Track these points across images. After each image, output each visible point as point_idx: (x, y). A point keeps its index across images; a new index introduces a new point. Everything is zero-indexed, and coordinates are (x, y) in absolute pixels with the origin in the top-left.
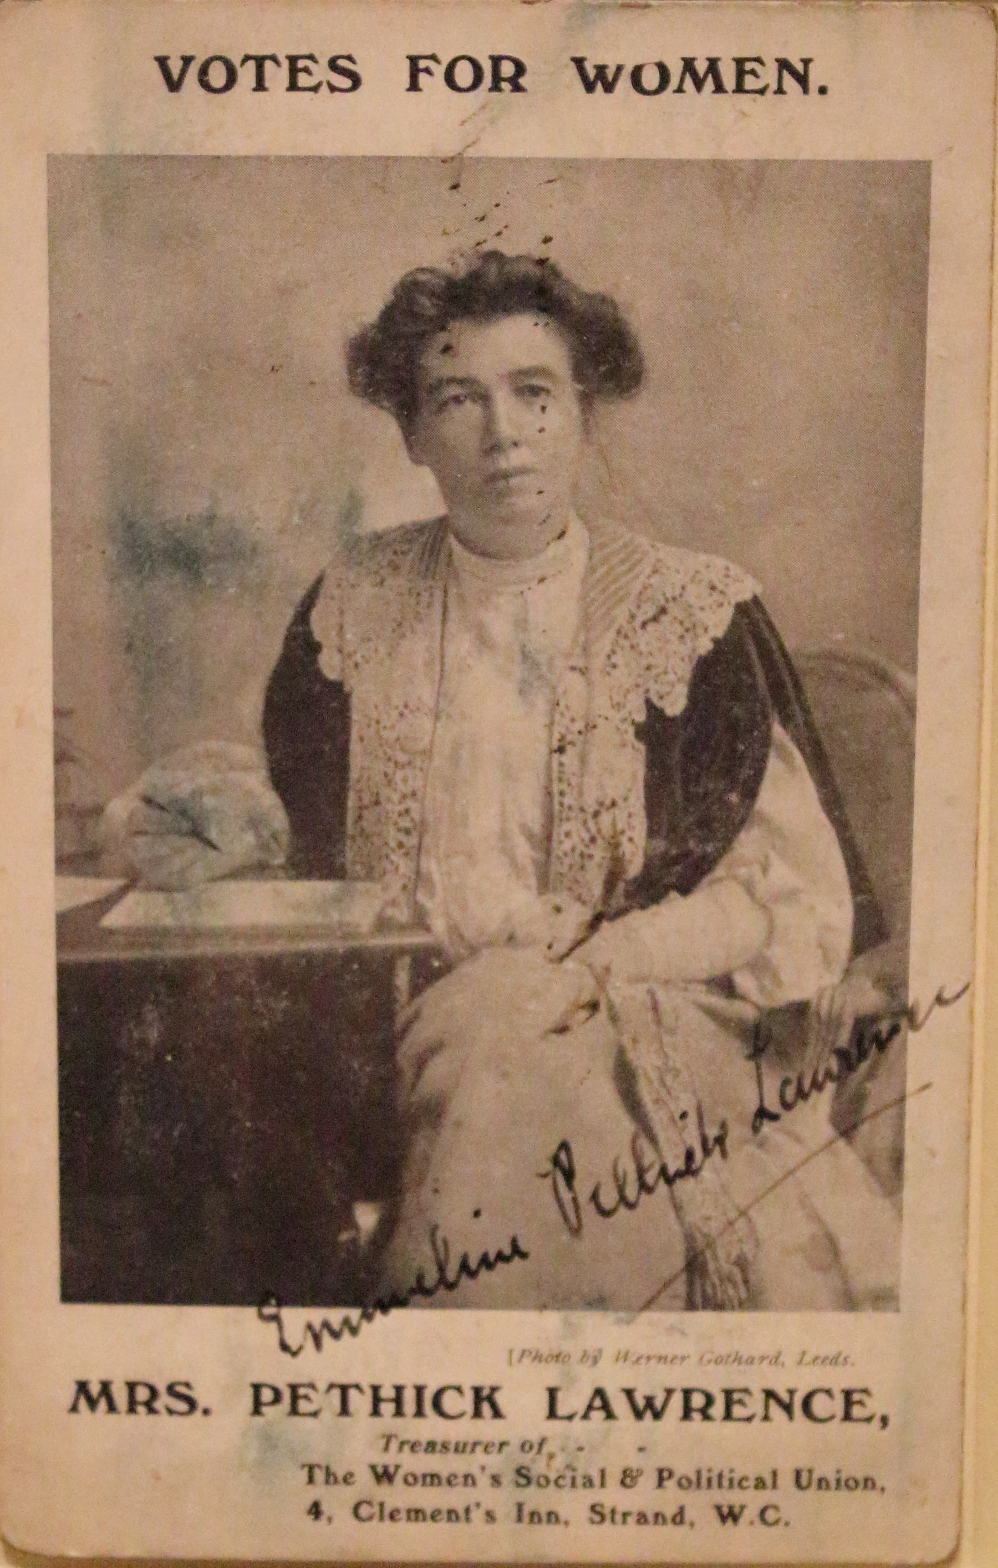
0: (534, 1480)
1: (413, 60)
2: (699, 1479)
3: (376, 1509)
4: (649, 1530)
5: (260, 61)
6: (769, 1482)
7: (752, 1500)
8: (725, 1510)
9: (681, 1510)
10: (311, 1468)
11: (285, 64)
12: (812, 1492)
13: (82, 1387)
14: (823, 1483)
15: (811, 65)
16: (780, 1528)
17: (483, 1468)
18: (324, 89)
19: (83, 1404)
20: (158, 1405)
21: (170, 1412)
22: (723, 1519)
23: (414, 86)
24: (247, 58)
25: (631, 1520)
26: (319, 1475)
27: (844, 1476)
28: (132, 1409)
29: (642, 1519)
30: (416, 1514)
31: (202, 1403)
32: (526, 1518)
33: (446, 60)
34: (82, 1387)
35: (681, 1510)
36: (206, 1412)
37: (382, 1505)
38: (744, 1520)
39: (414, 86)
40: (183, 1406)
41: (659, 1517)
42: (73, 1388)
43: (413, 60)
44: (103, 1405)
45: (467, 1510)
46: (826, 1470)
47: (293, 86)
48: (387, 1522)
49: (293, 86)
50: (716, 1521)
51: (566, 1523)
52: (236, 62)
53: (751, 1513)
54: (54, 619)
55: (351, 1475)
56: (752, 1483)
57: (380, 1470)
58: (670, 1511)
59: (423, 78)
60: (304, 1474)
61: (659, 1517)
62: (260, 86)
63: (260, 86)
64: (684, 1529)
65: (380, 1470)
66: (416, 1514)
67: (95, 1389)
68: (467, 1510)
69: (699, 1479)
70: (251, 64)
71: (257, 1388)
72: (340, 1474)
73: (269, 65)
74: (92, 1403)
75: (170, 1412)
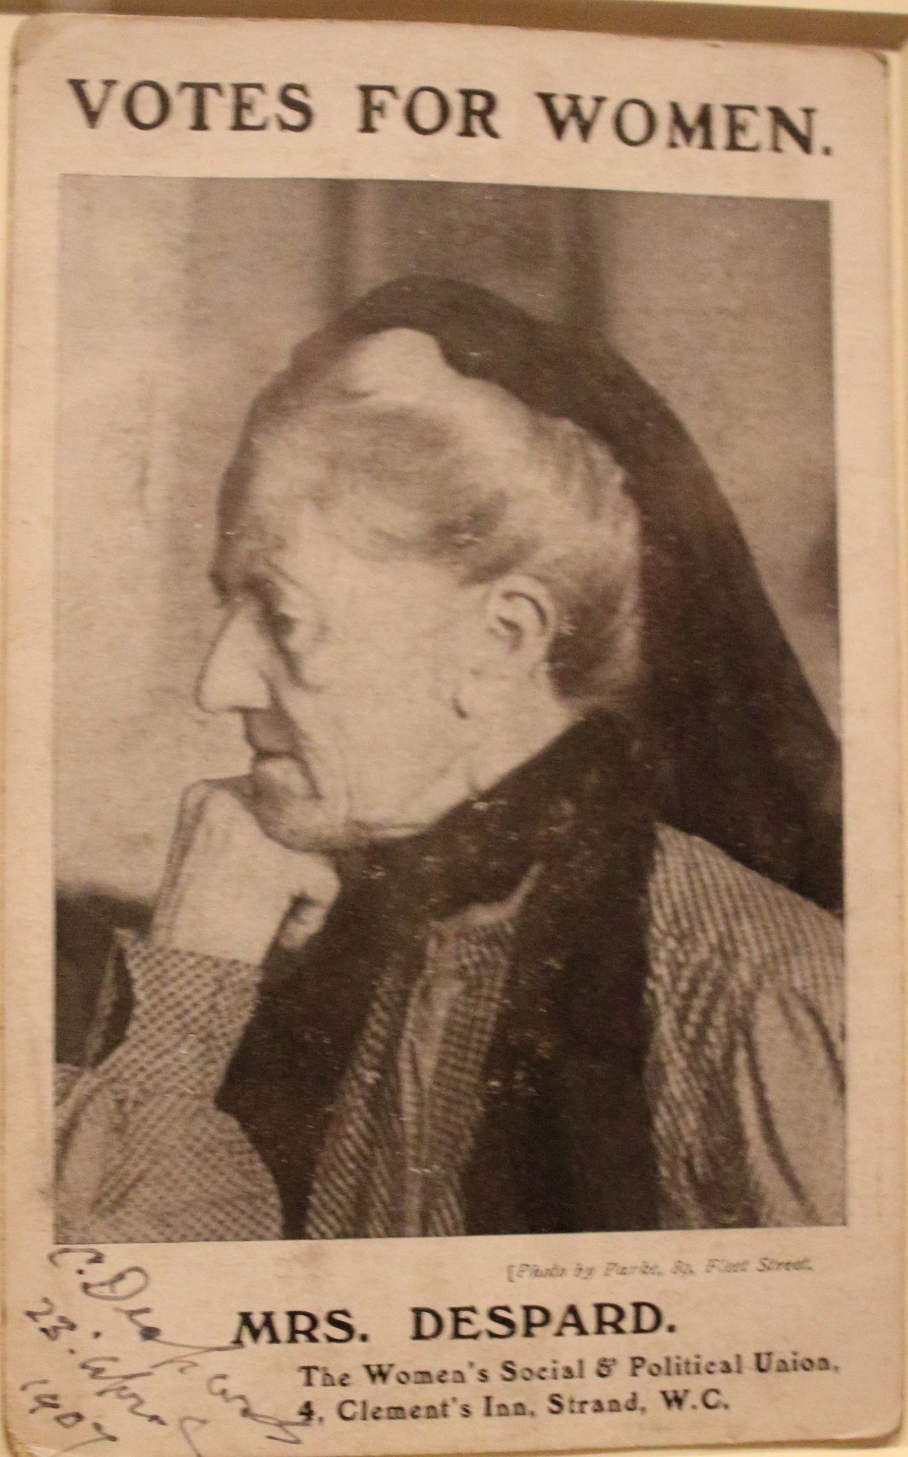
0: (519, 1374)
1: (366, 91)
2: (668, 1367)
3: (358, 1409)
4: (605, 1417)
5: (200, 90)
6: (734, 1367)
7: (697, 1384)
8: (671, 1395)
9: (634, 1398)
10: (308, 1369)
11: (229, 92)
12: (772, 1376)
13: (246, 1319)
14: (783, 1367)
15: (816, 117)
16: (720, 1411)
17: (471, 1364)
18: (274, 127)
19: (246, 1337)
20: (317, 1333)
21: (330, 1339)
22: (669, 1402)
23: (368, 127)
24: (185, 85)
25: (588, 1408)
26: (317, 1377)
27: (799, 1358)
28: (293, 1340)
29: (599, 1407)
30: (397, 1412)
31: (359, 1330)
32: (494, 1410)
33: (404, 93)
34: (246, 1319)
35: (634, 1398)
36: (364, 1338)
37: (364, 1403)
38: (687, 1405)
39: (368, 127)
40: (341, 1334)
41: (615, 1405)
42: (236, 1320)
43: (366, 91)
44: (265, 1335)
45: (445, 1405)
46: (783, 1352)
47: (239, 125)
48: (371, 1421)
49: (239, 125)
50: (662, 1403)
51: (532, 1414)
52: (171, 88)
53: (694, 1398)
54: (778, 624)
55: (346, 1376)
56: (719, 1367)
57: (374, 1369)
58: (624, 1398)
59: (377, 121)
60: (302, 1376)
61: (615, 1405)
62: (200, 124)
63: (200, 124)
64: (635, 1414)
65: (374, 1369)
66: (397, 1412)
67: (257, 1320)
68: (445, 1405)
69: (668, 1367)
70: (190, 93)
71: (418, 1312)
72: (336, 1375)
73: (211, 93)
74: (255, 1334)
75: (330, 1339)
